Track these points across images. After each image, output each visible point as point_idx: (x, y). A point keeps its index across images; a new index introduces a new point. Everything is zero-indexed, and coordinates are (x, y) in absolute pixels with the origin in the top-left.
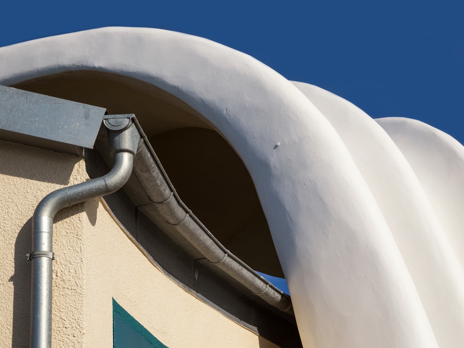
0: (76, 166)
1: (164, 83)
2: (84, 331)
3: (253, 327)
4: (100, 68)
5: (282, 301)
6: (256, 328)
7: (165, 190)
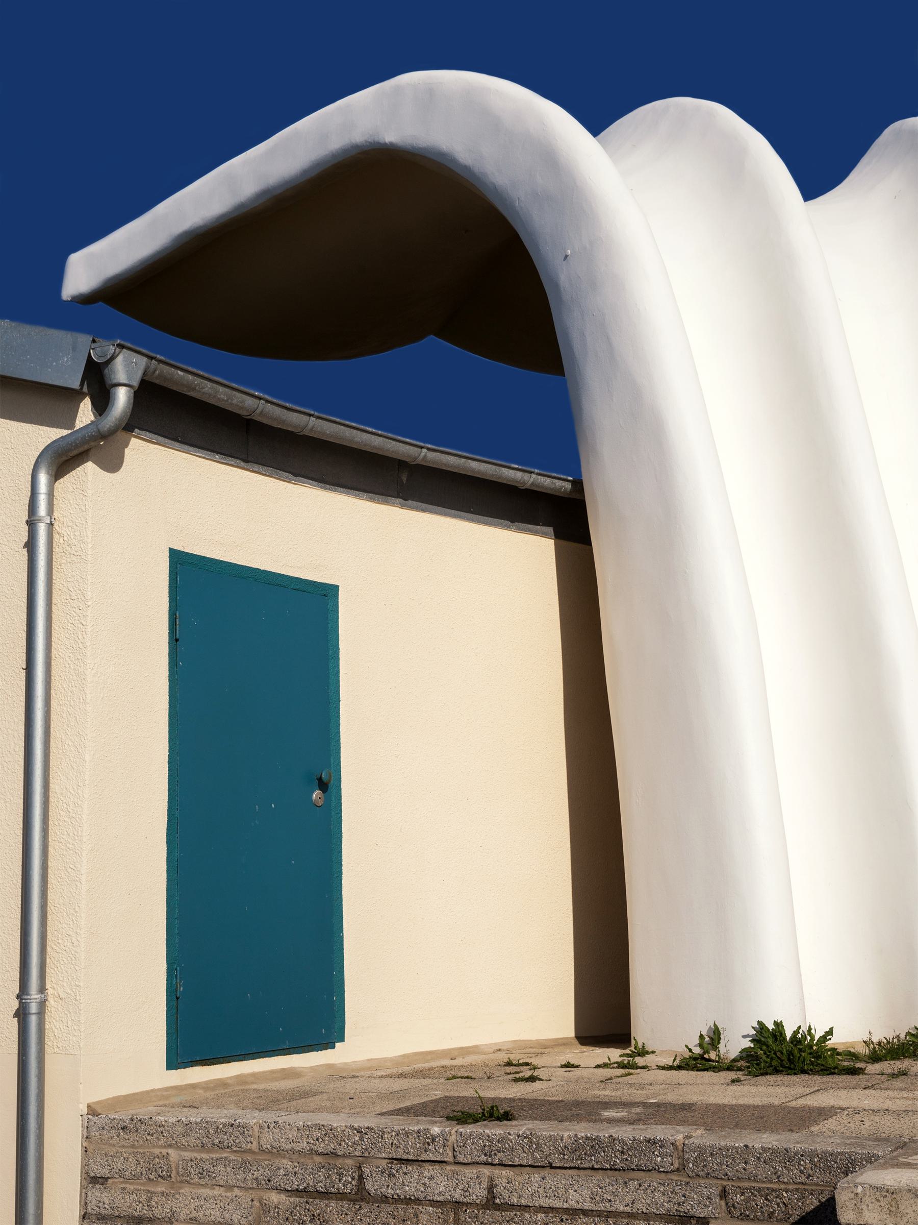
0: (82, 405)
1: (454, 161)
2: (89, 603)
3: (544, 528)
4: (391, 144)
5: (572, 491)
6: (550, 530)
7: (243, 402)
